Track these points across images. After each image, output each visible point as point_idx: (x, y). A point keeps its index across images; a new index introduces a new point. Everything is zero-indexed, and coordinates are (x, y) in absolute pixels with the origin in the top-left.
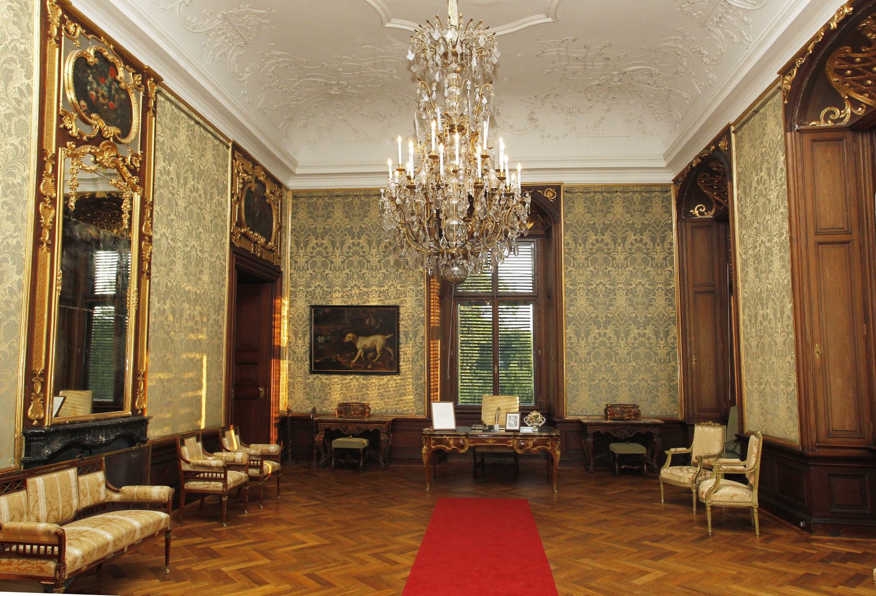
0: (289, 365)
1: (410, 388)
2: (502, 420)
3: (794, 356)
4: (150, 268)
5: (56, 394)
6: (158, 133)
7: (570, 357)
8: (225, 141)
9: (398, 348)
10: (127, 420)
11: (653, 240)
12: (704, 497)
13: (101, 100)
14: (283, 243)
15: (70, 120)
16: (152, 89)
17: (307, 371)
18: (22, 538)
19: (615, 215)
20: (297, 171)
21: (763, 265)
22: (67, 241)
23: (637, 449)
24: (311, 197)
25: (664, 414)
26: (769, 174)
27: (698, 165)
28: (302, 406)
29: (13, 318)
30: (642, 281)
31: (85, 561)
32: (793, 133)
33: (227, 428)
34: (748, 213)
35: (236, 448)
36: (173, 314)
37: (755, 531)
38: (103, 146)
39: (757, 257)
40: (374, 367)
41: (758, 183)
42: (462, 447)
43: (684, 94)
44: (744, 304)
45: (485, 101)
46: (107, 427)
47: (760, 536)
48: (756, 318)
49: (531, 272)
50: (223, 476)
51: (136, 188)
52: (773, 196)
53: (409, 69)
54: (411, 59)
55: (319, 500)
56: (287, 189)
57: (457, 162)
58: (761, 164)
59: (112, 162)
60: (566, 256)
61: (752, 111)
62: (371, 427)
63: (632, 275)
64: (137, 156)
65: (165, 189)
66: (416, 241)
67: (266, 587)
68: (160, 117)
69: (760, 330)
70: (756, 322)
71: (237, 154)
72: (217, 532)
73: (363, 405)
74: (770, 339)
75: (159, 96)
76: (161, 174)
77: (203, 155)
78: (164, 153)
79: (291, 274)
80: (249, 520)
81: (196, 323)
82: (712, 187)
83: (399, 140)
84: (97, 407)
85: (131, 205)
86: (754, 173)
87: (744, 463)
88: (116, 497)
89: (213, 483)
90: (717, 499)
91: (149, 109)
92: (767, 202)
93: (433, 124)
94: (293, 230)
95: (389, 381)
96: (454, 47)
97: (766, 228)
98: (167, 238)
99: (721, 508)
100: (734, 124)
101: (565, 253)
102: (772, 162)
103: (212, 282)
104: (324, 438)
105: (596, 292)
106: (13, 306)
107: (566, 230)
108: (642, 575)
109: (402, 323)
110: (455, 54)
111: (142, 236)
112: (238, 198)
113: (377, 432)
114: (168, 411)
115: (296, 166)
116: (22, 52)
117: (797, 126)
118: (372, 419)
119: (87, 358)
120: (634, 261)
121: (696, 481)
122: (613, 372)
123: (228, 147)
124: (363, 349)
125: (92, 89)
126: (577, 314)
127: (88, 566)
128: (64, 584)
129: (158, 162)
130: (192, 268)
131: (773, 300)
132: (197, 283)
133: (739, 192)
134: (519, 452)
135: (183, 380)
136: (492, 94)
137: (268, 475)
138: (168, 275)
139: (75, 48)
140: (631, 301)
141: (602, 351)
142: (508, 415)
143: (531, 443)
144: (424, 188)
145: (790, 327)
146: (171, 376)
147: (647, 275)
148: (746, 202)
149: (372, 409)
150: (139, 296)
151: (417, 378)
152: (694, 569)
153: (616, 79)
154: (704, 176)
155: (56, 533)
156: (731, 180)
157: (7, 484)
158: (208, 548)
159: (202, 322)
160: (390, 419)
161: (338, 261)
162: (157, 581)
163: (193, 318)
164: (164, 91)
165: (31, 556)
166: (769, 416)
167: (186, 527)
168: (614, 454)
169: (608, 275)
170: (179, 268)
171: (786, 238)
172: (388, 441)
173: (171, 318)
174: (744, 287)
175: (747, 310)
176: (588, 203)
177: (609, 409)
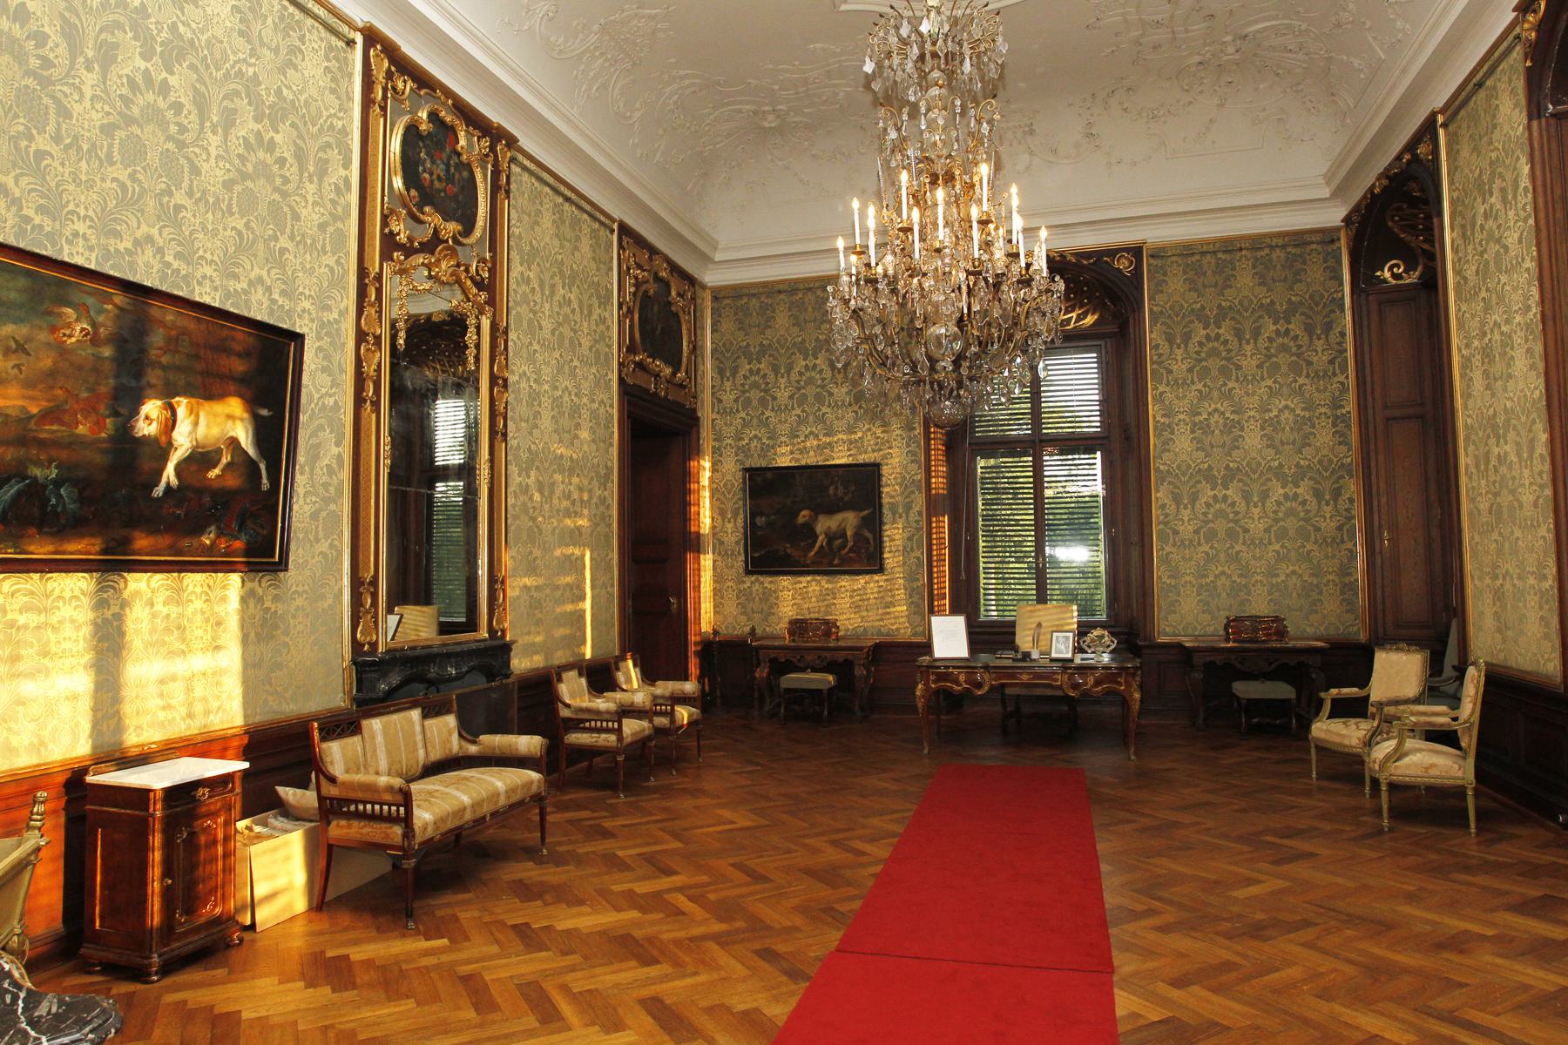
0: (714, 561)
1: (901, 594)
2: (1043, 644)
3: (1552, 526)
4: (505, 425)
5: (390, 611)
6: (513, 222)
7: (1163, 538)
8: (607, 222)
9: (881, 530)
10: (482, 645)
11: (1309, 330)
12: (1377, 767)
13: (437, 184)
14: (700, 372)
15: (398, 220)
16: (503, 158)
17: (741, 570)
18: (360, 795)
19: (1239, 290)
20: (718, 257)
21: (1498, 367)
22: (397, 393)
23: (1282, 690)
24: (740, 297)
25: (1332, 632)
26: (1504, 200)
27: (1385, 189)
28: (738, 626)
29: (333, 507)
30: (1219, 406)
31: (438, 828)
32: (1543, 120)
33: (623, 658)
34: (1470, 272)
35: (635, 685)
36: (540, 490)
37: (1468, 826)
38: (442, 251)
39: (1487, 353)
40: (843, 561)
41: (1486, 216)
42: (979, 685)
43: (1356, 62)
44: (1467, 439)
45: (985, 127)
46: (457, 655)
47: (1477, 835)
48: (1487, 463)
49: (1097, 397)
50: (616, 725)
51: (484, 308)
52: (1511, 239)
53: (867, 86)
54: (870, 72)
55: (757, 764)
56: (704, 287)
57: (943, 235)
58: (1491, 181)
59: (452, 275)
60: (1155, 366)
61: (1471, 86)
62: (840, 657)
63: (1273, 393)
64: (484, 261)
65: (524, 306)
66: (884, 364)
67: (674, 878)
68: (515, 198)
69: (1494, 482)
70: (1487, 470)
71: (625, 240)
72: (611, 805)
73: (827, 622)
74: (1511, 498)
75: (512, 166)
76: (518, 283)
77: (576, 248)
78: (521, 252)
79: (713, 420)
80: (655, 790)
81: (573, 503)
82: (1414, 227)
83: (856, 204)
84: (445, 628)
85: (478, 334)
86: (1479, 200)
87: (1454, 714)
88: (473, 749)
89: (603, 736)
90: (1399, 772)
91: (499, 188)
92: (1502, 250)
93: (904, 176)
94: (714, 351)
95: (867, 585)
96: (934, 44)
97: (1501, 299)
98: (528, 380)
99: (1419, 787)
100: (1443, 111)
101: (1152, 363)
102: (1509, 176)
103: (594, 441)
104: (769, 674)
105: (1208, 426)
106: (332, 490)
107: (1154, 321)
108: (1249, 885)
109: (885, 490)
110: (935, 55)
111: (493, 380)
112: (629, 308)
113: (848, 664)
114: (538, 633)
115: (715, 248)
116: (340, 132)
117: (1550, 107)
118: (842, 643)
119: (429, 558)
120: (1275, 368)
121: (1369, 743)
122: (1239, 561)
123: (612, 231)
124: (826, 534)
125: (425, 171)
126: (1244, 463)
127: (442, 835)
128: (414, 856)
129: (513, 265)
130: (565, 422)
131: (1515, 428)
132: (572, 444)
133: (1455, 234)
134: (1072, 694)
135: (558, 587)
136: (997, 117)
137: (682, 726)
138: (531, 433)
139: (405, 113)
140: (1270, 438)
141: (1221, 526)
142: (1055, 634)
143: (1091, 680)
144: (892, 282)
145: (1545, 476)
146: (541, 581)
147: (1300, 392)
148: (1466, 254)
149: (842, 628)
150: (492, 468)
151: (911, 577)
152: (1340, 880)
153: (1231, 50)
154: (1399, 209)
155: (401, 790)
156: (1440, 214)
157: (338, 727)
158: (599, 825)
159: (582, 501)
160: (870, 643)
161: (783, 395)
162: (530, 864)
163: (568, 496)
164: (520, 157)
165: (373, 817)
166: (1510, 633)
167: (568, 797)
168: (1238, 699)
169: (1228, 395)
170: (546, 422)
171: (1535, 314)
172: (867, 678)
173: (537, 496)
174: (1466, 407)
175: (1471, 448)
176: (1191, 274)
177: (1234, 624)
